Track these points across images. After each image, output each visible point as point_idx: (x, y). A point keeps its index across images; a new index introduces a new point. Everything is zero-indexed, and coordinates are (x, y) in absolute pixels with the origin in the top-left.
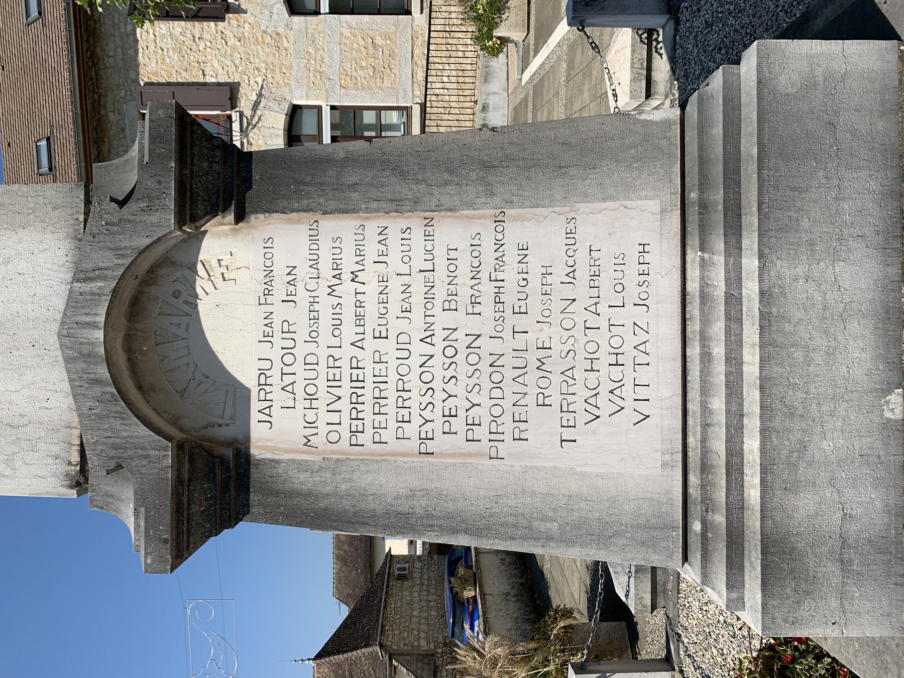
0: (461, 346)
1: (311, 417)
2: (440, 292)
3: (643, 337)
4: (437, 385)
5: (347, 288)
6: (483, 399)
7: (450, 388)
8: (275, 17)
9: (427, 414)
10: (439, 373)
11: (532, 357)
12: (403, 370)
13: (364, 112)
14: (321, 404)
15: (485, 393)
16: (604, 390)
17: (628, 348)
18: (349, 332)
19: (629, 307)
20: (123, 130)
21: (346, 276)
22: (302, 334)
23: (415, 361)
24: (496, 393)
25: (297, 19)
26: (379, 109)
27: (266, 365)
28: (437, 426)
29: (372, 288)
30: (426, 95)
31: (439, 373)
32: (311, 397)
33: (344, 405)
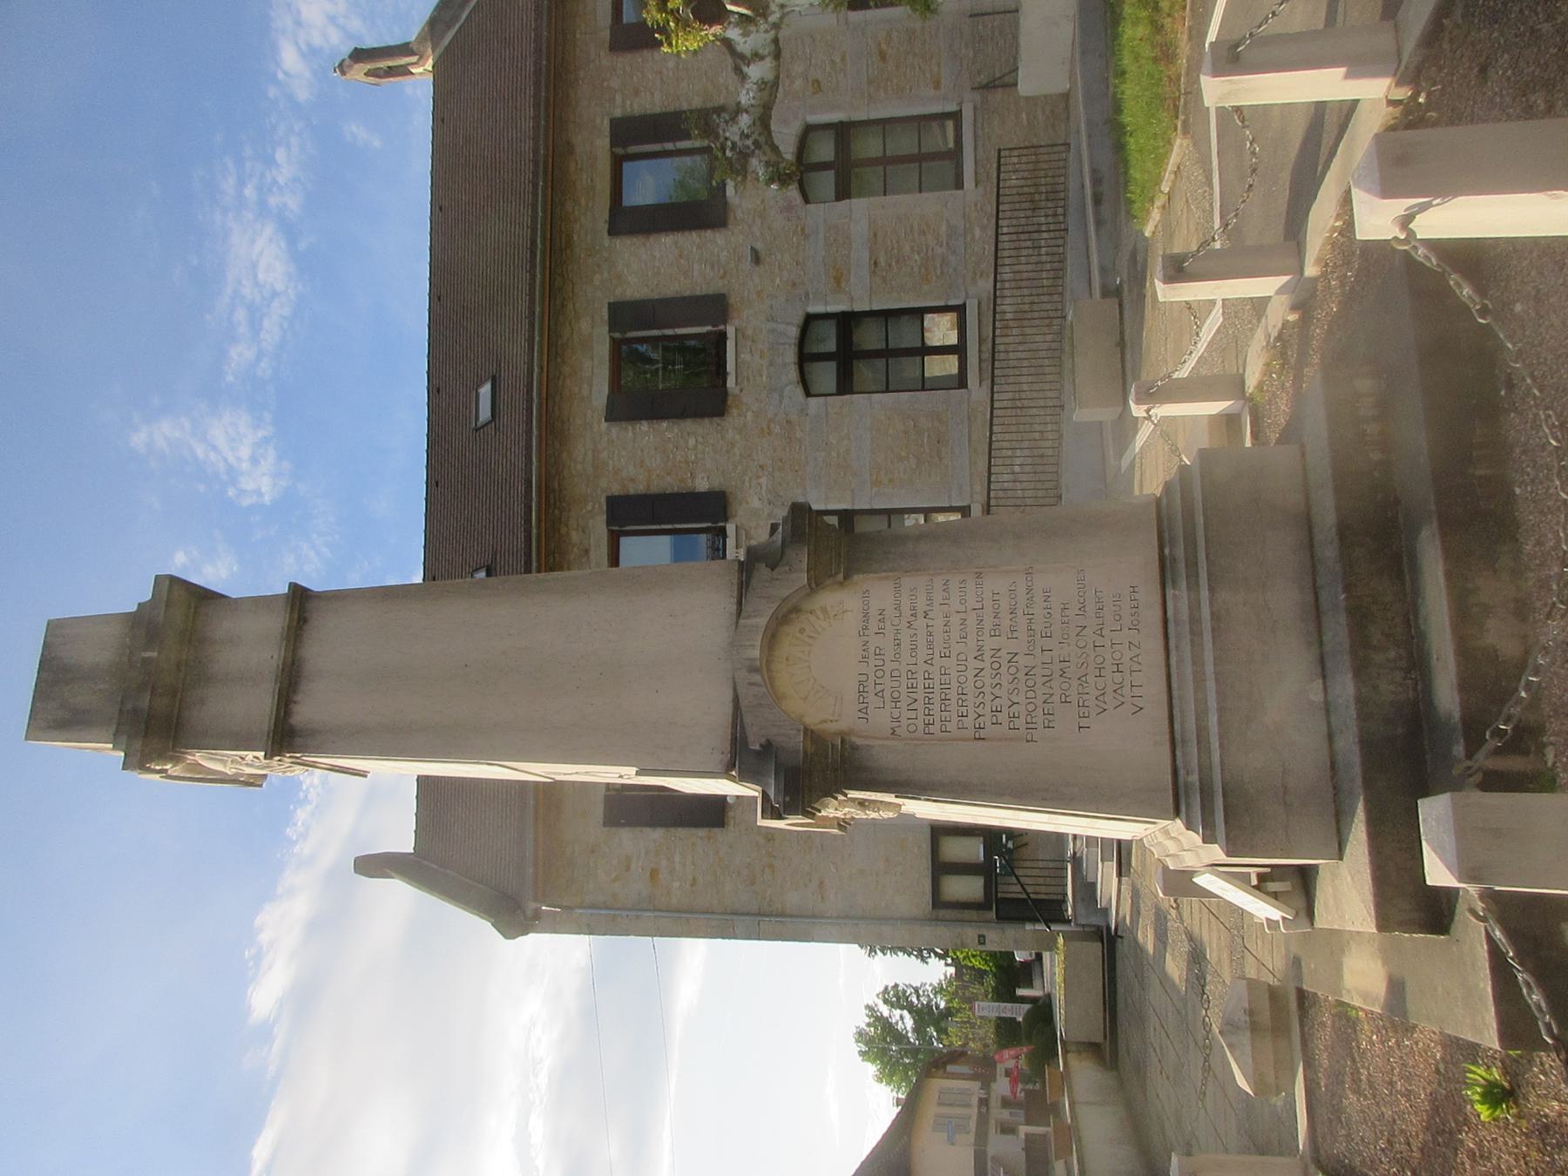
0: (1004, 662)
1: (896, 713)
2: (988, 623)
3: (1137, 651)
4: (987, 689)
5: (920, 623)
6: (1021, 698)
7: (997, 691)
8: (786, 401)
9: (980, 711)
10: (988, 681)
11: (1056, 667)
12: (962, 679)
13: (407, 846)
14: (903, 705)
15: (1022, 695)
16: (1109, 690)
17: (1126, 659)
18: (923, 653)
19: (1125, 630)
20: (587, 551)
21: (920, 614)
22: (889, 655)
23: (970, 673)
24: (1030, 694)
25: (812, 401)
26: (927, 512)
27: (863, 678)
28: (987, 720)
29: (938, 623)
30: (989, 490)
31: (988, 681)
32: (896, 701)
33: (919, 705)
